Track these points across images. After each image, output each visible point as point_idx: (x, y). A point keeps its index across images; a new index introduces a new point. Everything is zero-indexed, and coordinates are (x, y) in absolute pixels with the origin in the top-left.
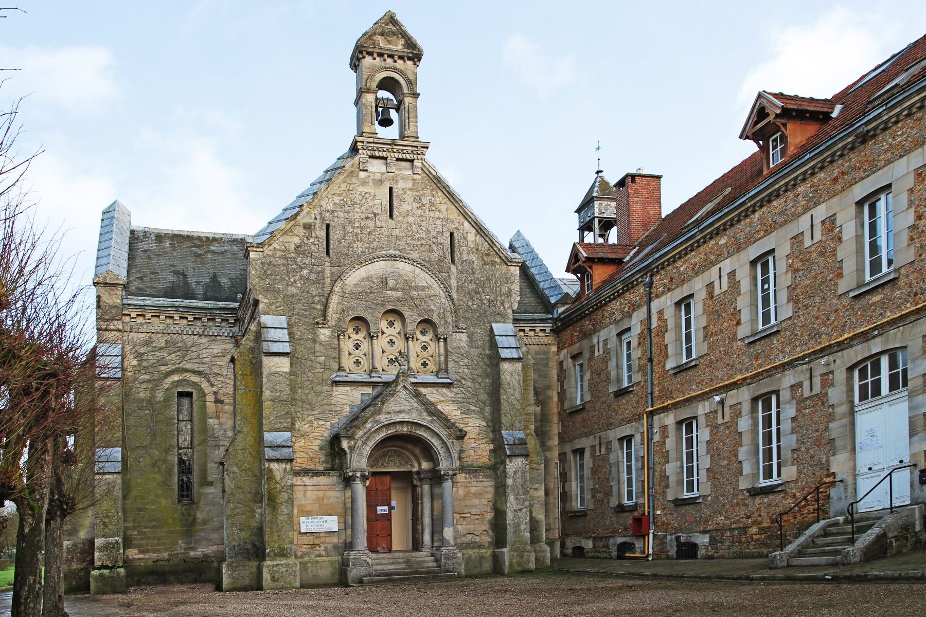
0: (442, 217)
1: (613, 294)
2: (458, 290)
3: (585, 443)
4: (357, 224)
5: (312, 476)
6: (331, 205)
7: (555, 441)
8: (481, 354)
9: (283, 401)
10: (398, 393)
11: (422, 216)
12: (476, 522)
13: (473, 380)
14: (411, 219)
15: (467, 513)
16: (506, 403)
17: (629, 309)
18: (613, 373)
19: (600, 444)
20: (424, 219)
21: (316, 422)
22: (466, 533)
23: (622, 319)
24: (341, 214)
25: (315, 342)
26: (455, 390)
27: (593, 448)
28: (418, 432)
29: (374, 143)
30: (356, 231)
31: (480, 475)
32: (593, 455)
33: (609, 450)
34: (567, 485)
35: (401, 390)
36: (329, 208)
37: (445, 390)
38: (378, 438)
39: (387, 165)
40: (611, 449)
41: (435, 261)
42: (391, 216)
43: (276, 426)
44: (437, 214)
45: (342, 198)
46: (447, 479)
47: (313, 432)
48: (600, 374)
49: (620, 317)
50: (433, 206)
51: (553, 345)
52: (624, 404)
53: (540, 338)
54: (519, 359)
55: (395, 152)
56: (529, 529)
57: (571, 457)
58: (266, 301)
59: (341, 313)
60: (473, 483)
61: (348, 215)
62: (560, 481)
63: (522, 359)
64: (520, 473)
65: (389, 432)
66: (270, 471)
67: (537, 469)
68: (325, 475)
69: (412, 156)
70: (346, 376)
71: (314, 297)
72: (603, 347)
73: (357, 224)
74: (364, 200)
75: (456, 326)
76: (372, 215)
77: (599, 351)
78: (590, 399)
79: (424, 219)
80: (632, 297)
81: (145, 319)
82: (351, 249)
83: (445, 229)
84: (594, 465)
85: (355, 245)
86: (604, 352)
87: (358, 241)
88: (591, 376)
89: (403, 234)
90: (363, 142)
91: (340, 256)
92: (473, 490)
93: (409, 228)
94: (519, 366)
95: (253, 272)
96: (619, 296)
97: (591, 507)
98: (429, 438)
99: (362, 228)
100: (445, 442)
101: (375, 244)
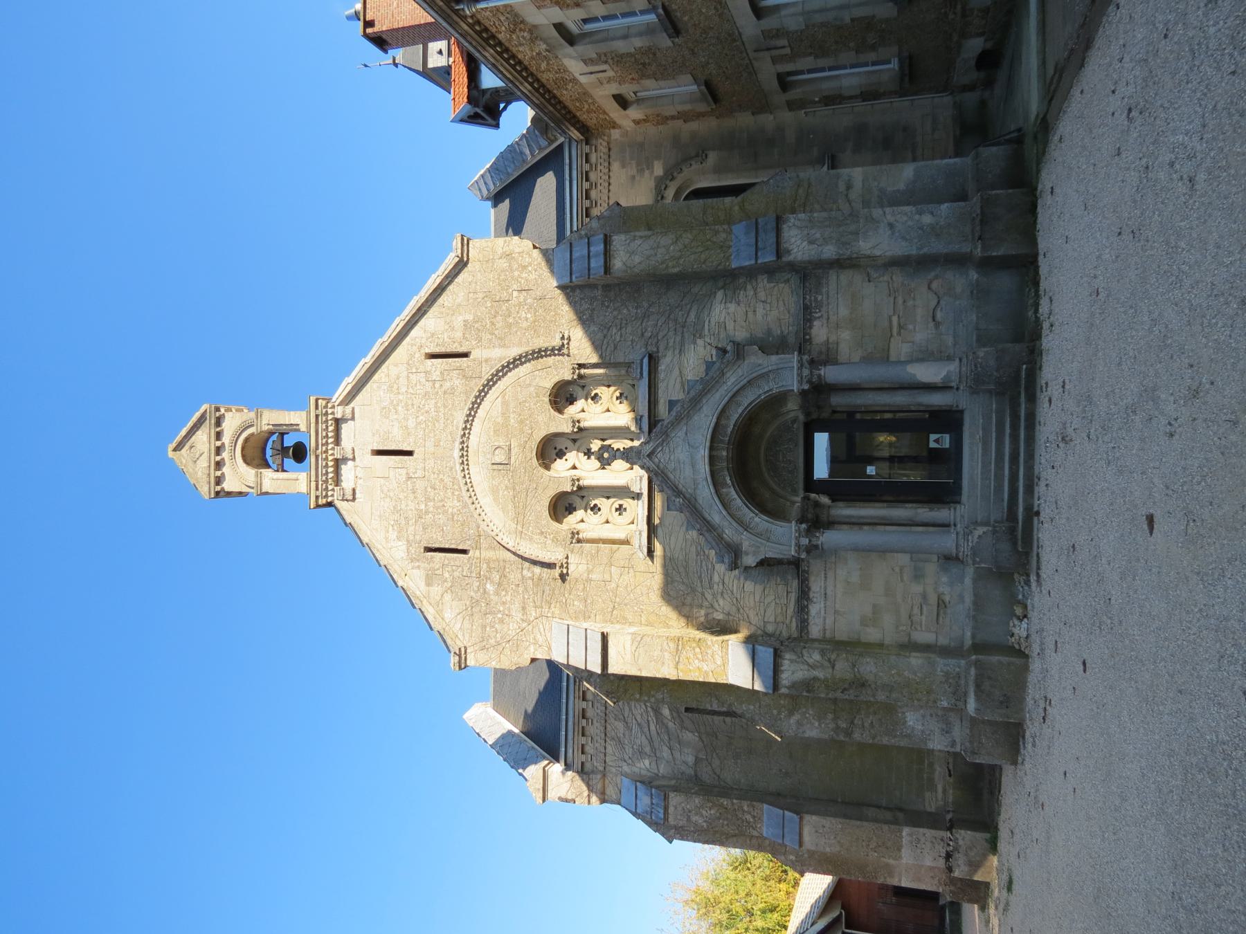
0: (405, 373)
1: (507, 60)
2: (504, 346)
3: (767, 72)
4: (423, 507)
5: (808, 599)
6: (400, 543)
7: (767, 120)
8: (603, 304)
9: (677, 650)
10: (661, 466)
11: (406, 405)
12: (910, 303)
13: (646, 316)
14: (411, 423)
15: (890, 321)
16: (681, 261)
17: (524, 31)
18: (638, 42)
19: (768, 49)
20: (410, 402)
21: (716, 587)
22: (932, 324)
23: (544, 40)
24: (411, 529)
25: (589, 580)
26: (661, 348)
27: (775, 60)
28: (730, 430)
29: (317, 481)
30: (432, 509)
31: (816, 299)
32: (791, 58)
33: (778, 33)
34: (846, 93)
35: (656, 460)
36: (404, 547)
37: (662, 367)
38: (739, 501)
39: (345, 460)
40: (778, 30)
41: (466, 385)
42: (410, 453)
43: (719, 663)
44: (403, 381)
45: (391, 528)
46: (819, 376)
47: (732, 592)
48: (644, 64)
49: (541, 43)
50: (392, 387)
51: (609, 136)
52: (691, 18)
53: (599, 160)
54: (607, 241)
55: (327, 449)
56: (931, 207)
57: (794, 94)
58: (532, 648)
59: (546, 537)
60: (831, 313)
61: (412, 519)
62: (840, 103)
63: (606, 236)
64: (813, 232)
65: (729, 482)
66: (793, 686)
67: (810, 185)
68: (807, 579)
69: (330, 422)
70: (640, 534)
71: (523, 577)
72: (597, 64)
73: (423, 507)
74: (392, 494)
75: (560, 350)
76: (409, 483)
77: (605, 71)
78: (689, 76)
79: (410, 402)
80: (503, 28)
81: (587, 743)
82: (455, 517)
83: (421, 369)
84: (810, 54)
85: (450, 510)
86: (606, 62)
87: (444, 506)
88: (648, 77)
89: (432, 435)
90: (317, 497)
91: (466, 533)
92: (844, 312)
93: (423, 426)
94: (618, 240)
95: (494, 663)
96: (507, 50)
97: (895, 49)
98: (740, 411)
99: (428, 499)
100: (749, 382)
101: (447, 480)
